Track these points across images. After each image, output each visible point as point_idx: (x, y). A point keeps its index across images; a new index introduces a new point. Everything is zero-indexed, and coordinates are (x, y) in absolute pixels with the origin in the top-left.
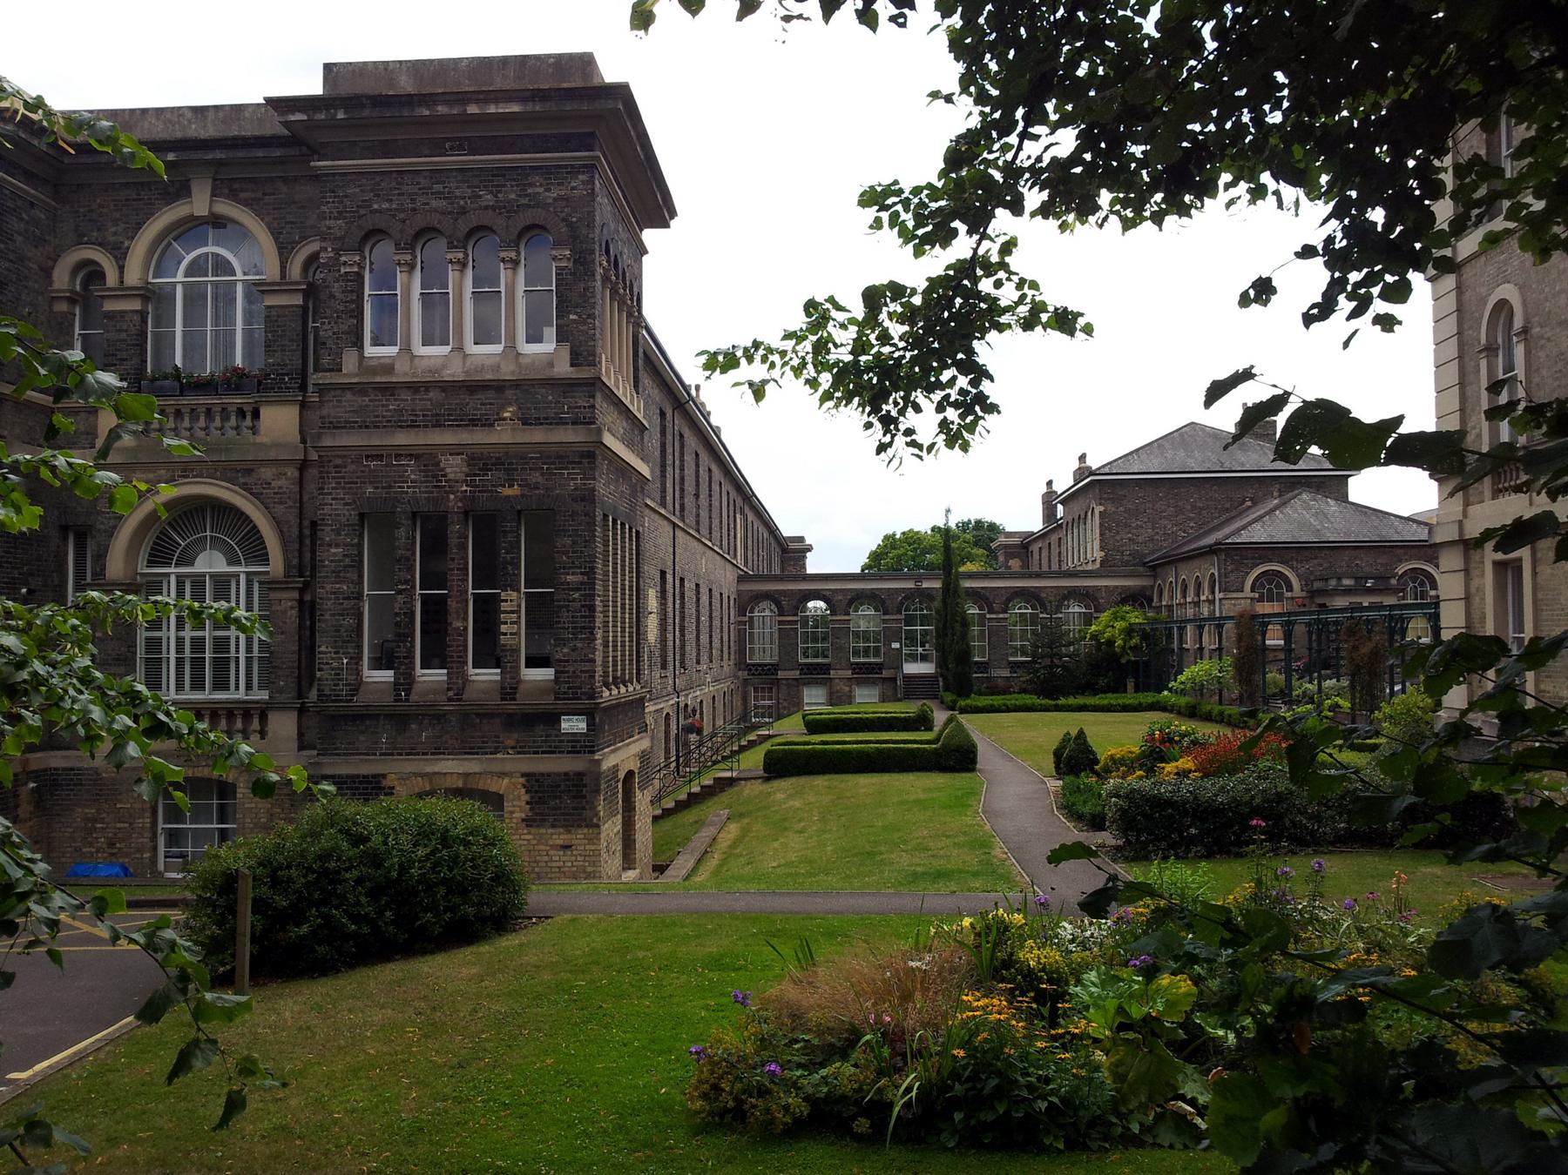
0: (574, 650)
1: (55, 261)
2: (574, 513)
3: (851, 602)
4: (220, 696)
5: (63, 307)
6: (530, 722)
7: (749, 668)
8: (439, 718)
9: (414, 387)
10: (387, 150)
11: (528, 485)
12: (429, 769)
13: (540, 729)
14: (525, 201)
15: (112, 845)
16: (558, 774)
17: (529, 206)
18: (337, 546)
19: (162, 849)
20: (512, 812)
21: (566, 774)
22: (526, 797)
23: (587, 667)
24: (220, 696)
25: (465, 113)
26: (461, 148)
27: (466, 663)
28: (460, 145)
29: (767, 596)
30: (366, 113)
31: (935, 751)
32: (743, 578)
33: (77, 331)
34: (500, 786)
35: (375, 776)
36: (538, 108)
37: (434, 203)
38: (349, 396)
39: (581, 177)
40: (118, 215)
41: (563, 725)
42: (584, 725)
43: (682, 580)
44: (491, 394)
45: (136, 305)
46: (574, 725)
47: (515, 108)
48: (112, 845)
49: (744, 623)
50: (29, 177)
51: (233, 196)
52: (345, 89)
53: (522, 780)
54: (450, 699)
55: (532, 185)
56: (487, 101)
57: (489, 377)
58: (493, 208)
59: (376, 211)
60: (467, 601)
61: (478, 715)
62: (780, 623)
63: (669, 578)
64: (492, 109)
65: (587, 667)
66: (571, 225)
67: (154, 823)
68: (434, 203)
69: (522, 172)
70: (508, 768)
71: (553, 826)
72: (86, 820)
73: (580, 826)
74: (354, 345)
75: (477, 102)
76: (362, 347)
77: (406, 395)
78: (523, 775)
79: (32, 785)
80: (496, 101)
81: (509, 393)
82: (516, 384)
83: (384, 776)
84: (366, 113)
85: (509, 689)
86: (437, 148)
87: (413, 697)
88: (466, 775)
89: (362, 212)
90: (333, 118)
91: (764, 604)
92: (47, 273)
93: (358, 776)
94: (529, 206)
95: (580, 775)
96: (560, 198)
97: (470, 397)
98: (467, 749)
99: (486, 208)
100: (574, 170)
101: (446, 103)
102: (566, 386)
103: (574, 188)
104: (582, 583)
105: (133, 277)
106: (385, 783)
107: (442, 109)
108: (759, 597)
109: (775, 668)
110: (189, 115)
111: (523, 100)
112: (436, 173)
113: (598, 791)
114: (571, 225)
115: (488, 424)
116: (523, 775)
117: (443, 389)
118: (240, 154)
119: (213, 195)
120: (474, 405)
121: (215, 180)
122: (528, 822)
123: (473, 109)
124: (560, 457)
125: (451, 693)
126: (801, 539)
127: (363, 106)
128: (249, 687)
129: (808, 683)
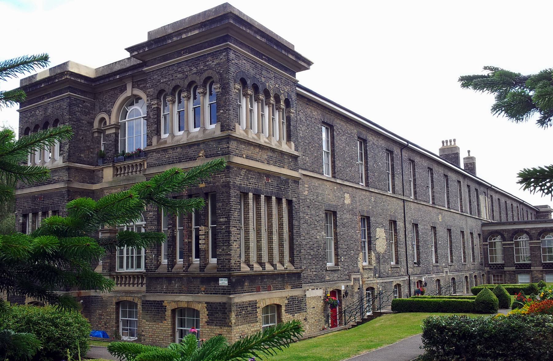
0: (223, 250)
1: (94, 119)
2: (223, 192)
3: (540, 234)
4: (138, 270)
5: (96, 135)
6: (209, 281)
7: (489, 266)
8: (181, 278)
9: (173, 148)
10: (165, 58)
11: (207, 183)
12: (177, 299)
13: (212, 284)
14: (205, 68)
15: (105, 324)
16: (217, 303)
17: (207, 70)
18: (151, 212)
19: (121, 327)
20: (202, 319)
21: (220, 303)
22: (207, 313)
23: (228, 257)
24: (138, 270)
25: (181, 39)
26: (186, 52)
27: (192, 256)
28: (190, 50)
29: (497, 233)
30: (153, 47)
31: (473, 303)
32: (484, 225)
33: (102, 143)
34: (198, 307)
35: (161, 301)
36: (204, 30)
37: (178, 76)
38: (155, 154)
39: (224, 54)
40: (109, 100)
41: (220, 282)
42: (226, 282)
43: (416, 225)
44: (196, 147)
45: (113, 131)
46: (223, 282)
47: (197, 32)
48: (105, 324)
49: (487, 245)
50: (83, 93)
51: (138, 88)
52: (153, 38)
53: (206, 305)
54: (184, 271)
55: (208, 61)
56: (188, 32)
57: (194, 140)
58: (196, 73)
59: (162, 83)
60: (191, 232)
61: (193, 277)
62: (504, 244)
63: (400, 224)
64: (190, 34)
65: (228, 257)
66: (221, 75)
67: (117, 317)
68: (178, 76)
69: (205, 56)
70: (201, 299)
71: (216, 325)
72: (99, 315)
73: (225, 326)
74: (157, 134)
75: (185, 33)
76: (160, 135)
77: (170, 151)
78: (206, 303)
79: (82, 301)
80: (191, 31)
81: (201, 146)
82: (204, 142)
83: (163, 301)
84: (153, 47)
85: (202, 268)
86: (179, 54)
87: (173, 270)
88: (188, 302)
89: (158, 84)
90: (145, 51)
91: (525, 235)
92: (91, 124)
93: (155, 301)
94: (207, 70)
95: (224, 303)
96: (218, 64)
97: (189, 149)
98: (190, 292)
99: (194, 73)
100: (221, 52)
101: (176, 36)
102: (219, 140)
103: (221, 59)
104: (226, 222)
105: (113, 121)
106: (164, 304)
107: (175, 39)
108: (494, 234)
109: (503, 266)
110: (126, 61)
111: (199, 28)
112: (179, 64)
113: (231, 311)
114: (221, 75)
115: (193, 159)
116: (206, 303)
117: (181, 148)
118: (136, 71)
119: (133, 87)
120: (191, 152)
121: (133, 82)
122: (208, 323)
123: (184, 36)
124: (217, 168)
125: (184, 269)
126: (546, 206)
127: (152, 44)
128: (127, 267)
129: (520, 273)
